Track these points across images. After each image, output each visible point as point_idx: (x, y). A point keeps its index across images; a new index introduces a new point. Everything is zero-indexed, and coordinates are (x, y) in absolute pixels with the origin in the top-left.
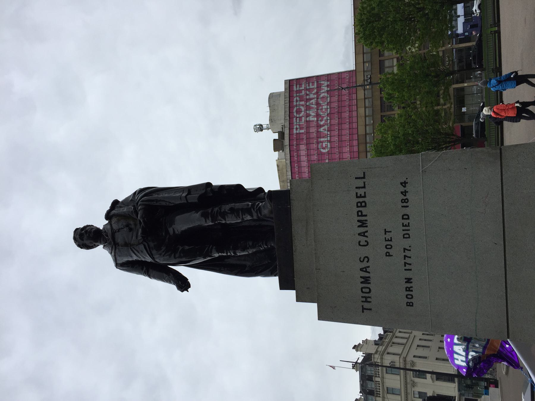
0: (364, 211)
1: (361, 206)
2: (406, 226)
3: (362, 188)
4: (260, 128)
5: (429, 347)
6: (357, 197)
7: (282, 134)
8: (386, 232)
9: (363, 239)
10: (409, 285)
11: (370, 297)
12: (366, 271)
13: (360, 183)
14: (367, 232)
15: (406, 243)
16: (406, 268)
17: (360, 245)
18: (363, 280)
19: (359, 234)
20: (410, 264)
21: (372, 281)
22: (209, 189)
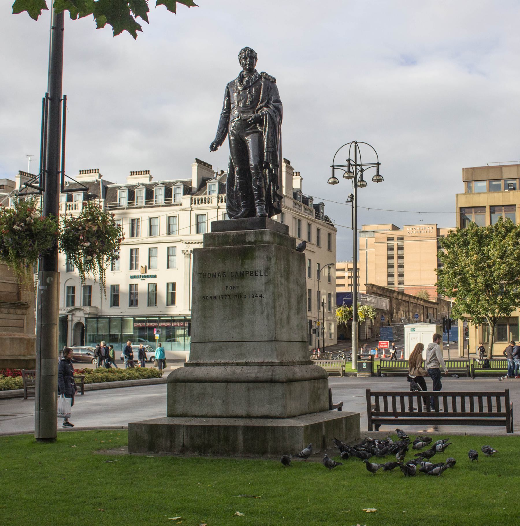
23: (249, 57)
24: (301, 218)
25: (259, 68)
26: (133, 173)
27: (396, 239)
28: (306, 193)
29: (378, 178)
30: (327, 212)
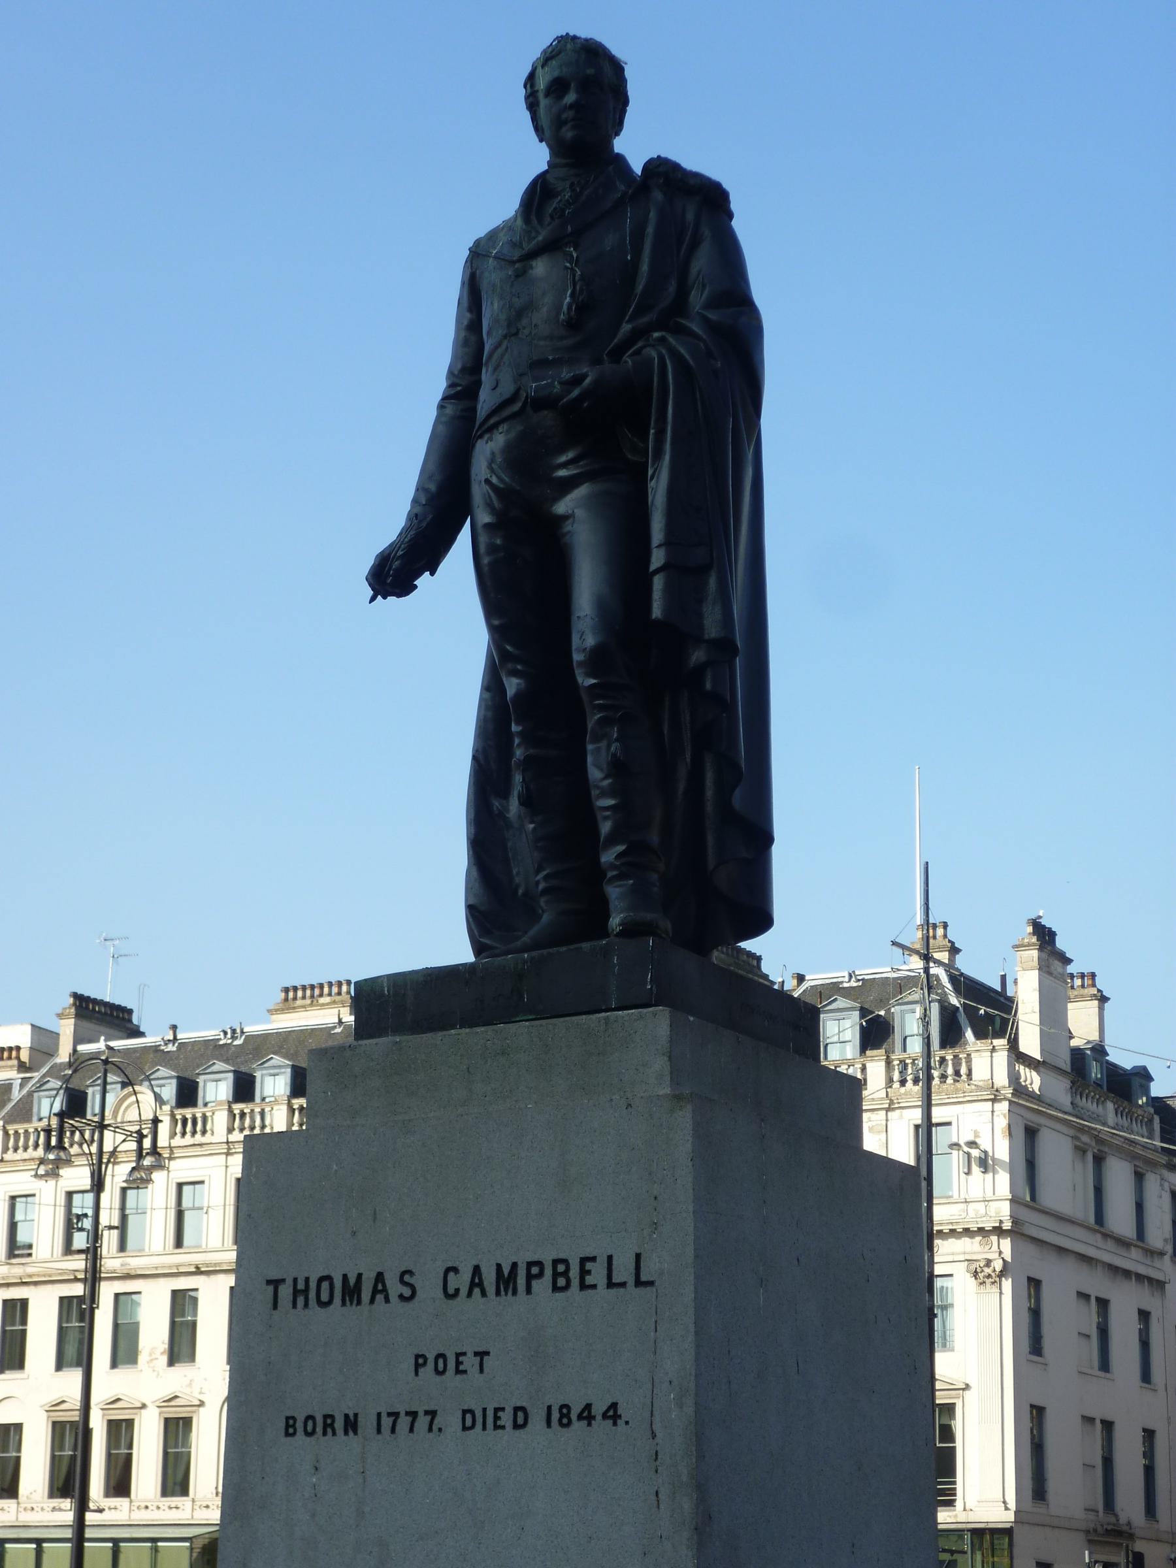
23: (579, 90)
24: (1042, 1120)
25: (635, 146)
26: (1149, 1435)
28: (1122, 1058)
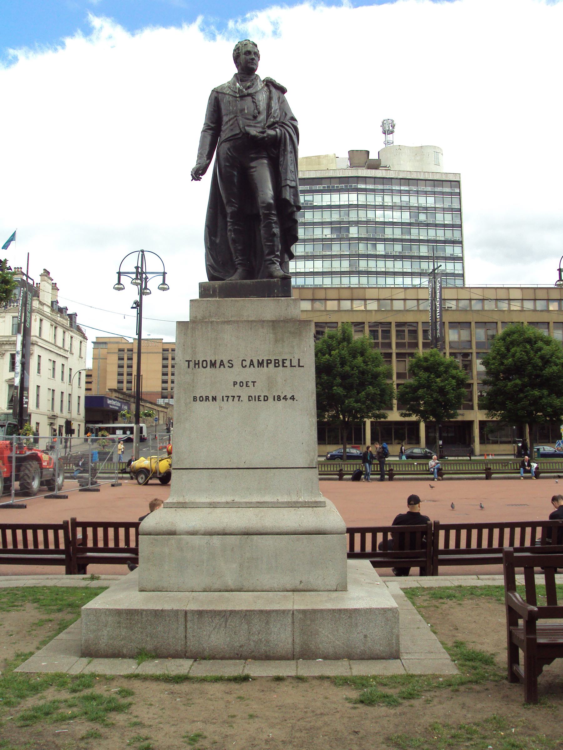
0: (271, 366)
1: (275, 363)
2: (259, 398)
3: (291, 364)
4: (388, 129)
5: (54, 377)
6: (283, 360)
7: (375, 165)
8: (254, 382)
9: (248, 363)
10: (211, 398)
11: (199, 367)
12: (221, 365)
13: (295, 363)
14: (254, 367)
15: (244, 398)
16: (224, 397)
17: (243, 360)
18: (213, 362)
19: (252, 361)
20: (227, 400)
21: (213, 369)
22: (295, 209)
27: (126, 351)
29: (164, 287)
30: (79, 320)
